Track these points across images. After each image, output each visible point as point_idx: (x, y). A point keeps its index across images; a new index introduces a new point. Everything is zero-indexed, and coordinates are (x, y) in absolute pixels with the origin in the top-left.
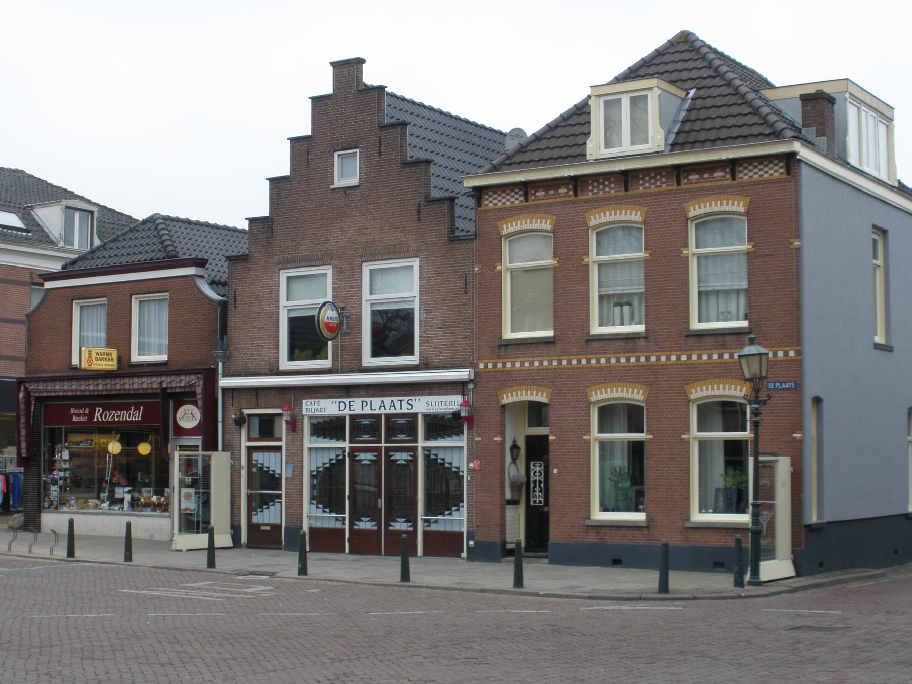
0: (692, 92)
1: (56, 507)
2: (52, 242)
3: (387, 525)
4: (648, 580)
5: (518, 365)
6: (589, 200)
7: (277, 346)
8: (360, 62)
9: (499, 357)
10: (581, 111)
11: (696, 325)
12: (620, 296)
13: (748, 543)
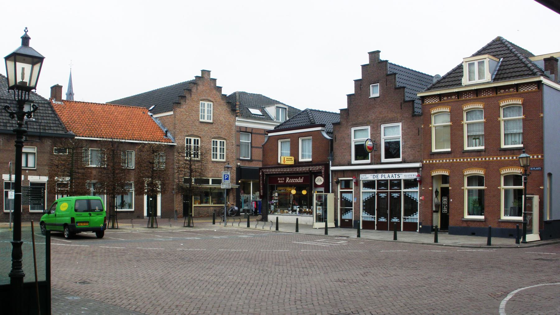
0: (502, 59)
1: (273, 213)
2: (272, 119)
3: (390, 220)
4: (483, 241)
5: (438, 161)
6: (462, 101)
7: (351, 155)
8: (378, 52)
9: (431, 159)
10: (460, 67)
11: (503, 146)
12: (475, 136)
13: (521, 227)
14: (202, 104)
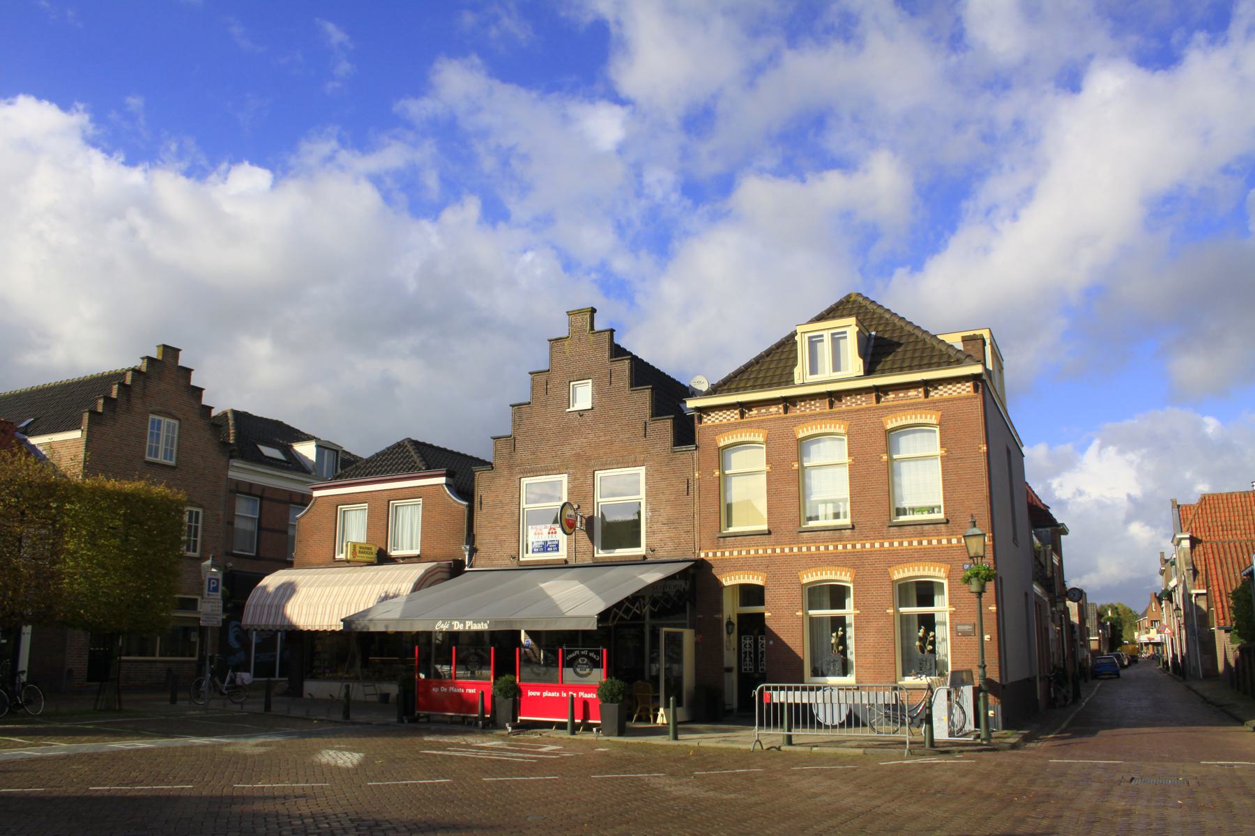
6: (798, 417)
14: (153, 422)
